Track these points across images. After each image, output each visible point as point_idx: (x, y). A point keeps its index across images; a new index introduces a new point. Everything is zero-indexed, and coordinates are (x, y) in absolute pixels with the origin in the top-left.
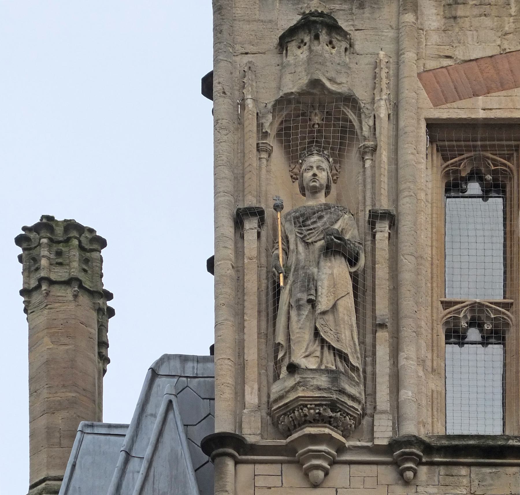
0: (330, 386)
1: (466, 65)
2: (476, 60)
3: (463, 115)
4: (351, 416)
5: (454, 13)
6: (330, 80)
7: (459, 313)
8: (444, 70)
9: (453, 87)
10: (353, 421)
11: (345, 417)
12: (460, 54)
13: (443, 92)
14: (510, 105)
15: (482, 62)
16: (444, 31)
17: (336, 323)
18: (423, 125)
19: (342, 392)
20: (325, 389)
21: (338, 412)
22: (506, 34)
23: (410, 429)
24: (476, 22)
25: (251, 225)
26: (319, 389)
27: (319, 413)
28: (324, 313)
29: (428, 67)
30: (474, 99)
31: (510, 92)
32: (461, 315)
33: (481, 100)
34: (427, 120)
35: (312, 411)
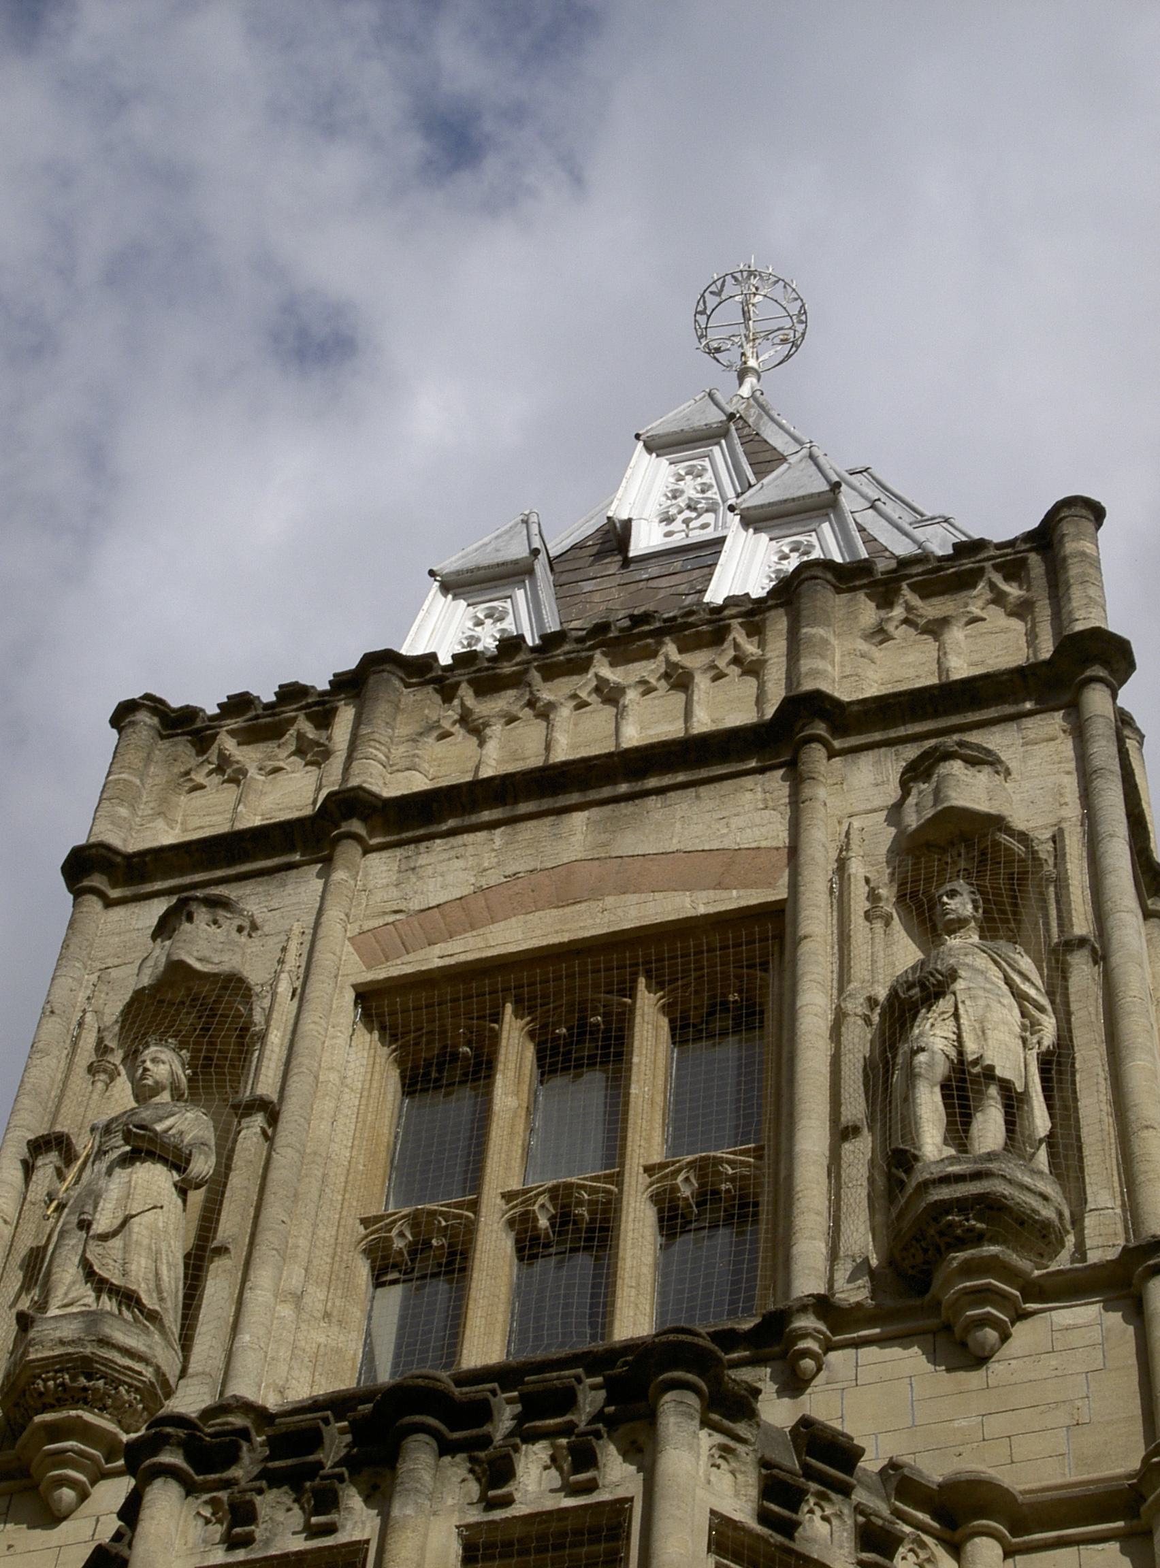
0: (82, 1335)
1: (422, 915)
2: (438, 906)
3: (409, 969)
4: (130, 1386)
5: (412, 865)
6: (200, 960)
7: (390, 1231)
8: (391, 927)
9: (398, 942)
10: (133, 1395)
11: (116, 1388)
12: (415, 905)
13: (383, 950)
14: (482, 945)
15: (446, 907)
16: (397, 885)
17: (126, 1248)
18: (350, 995)
19: (104, 1342)
20: (73, 1341)
21: (98, 1379)
22: (485, 870)
23: (243, 1388)
24: (442, 868)
25: (49, 1162)
26: (62, 1342)
27: (63, 1384)
28: (104, 1237)
29: (365, 928)
30: (428, 949)
31: (481, 931)
32: (394, 1233)
33: (437, 949)
34: (354, 986)
35: (51, 1383)
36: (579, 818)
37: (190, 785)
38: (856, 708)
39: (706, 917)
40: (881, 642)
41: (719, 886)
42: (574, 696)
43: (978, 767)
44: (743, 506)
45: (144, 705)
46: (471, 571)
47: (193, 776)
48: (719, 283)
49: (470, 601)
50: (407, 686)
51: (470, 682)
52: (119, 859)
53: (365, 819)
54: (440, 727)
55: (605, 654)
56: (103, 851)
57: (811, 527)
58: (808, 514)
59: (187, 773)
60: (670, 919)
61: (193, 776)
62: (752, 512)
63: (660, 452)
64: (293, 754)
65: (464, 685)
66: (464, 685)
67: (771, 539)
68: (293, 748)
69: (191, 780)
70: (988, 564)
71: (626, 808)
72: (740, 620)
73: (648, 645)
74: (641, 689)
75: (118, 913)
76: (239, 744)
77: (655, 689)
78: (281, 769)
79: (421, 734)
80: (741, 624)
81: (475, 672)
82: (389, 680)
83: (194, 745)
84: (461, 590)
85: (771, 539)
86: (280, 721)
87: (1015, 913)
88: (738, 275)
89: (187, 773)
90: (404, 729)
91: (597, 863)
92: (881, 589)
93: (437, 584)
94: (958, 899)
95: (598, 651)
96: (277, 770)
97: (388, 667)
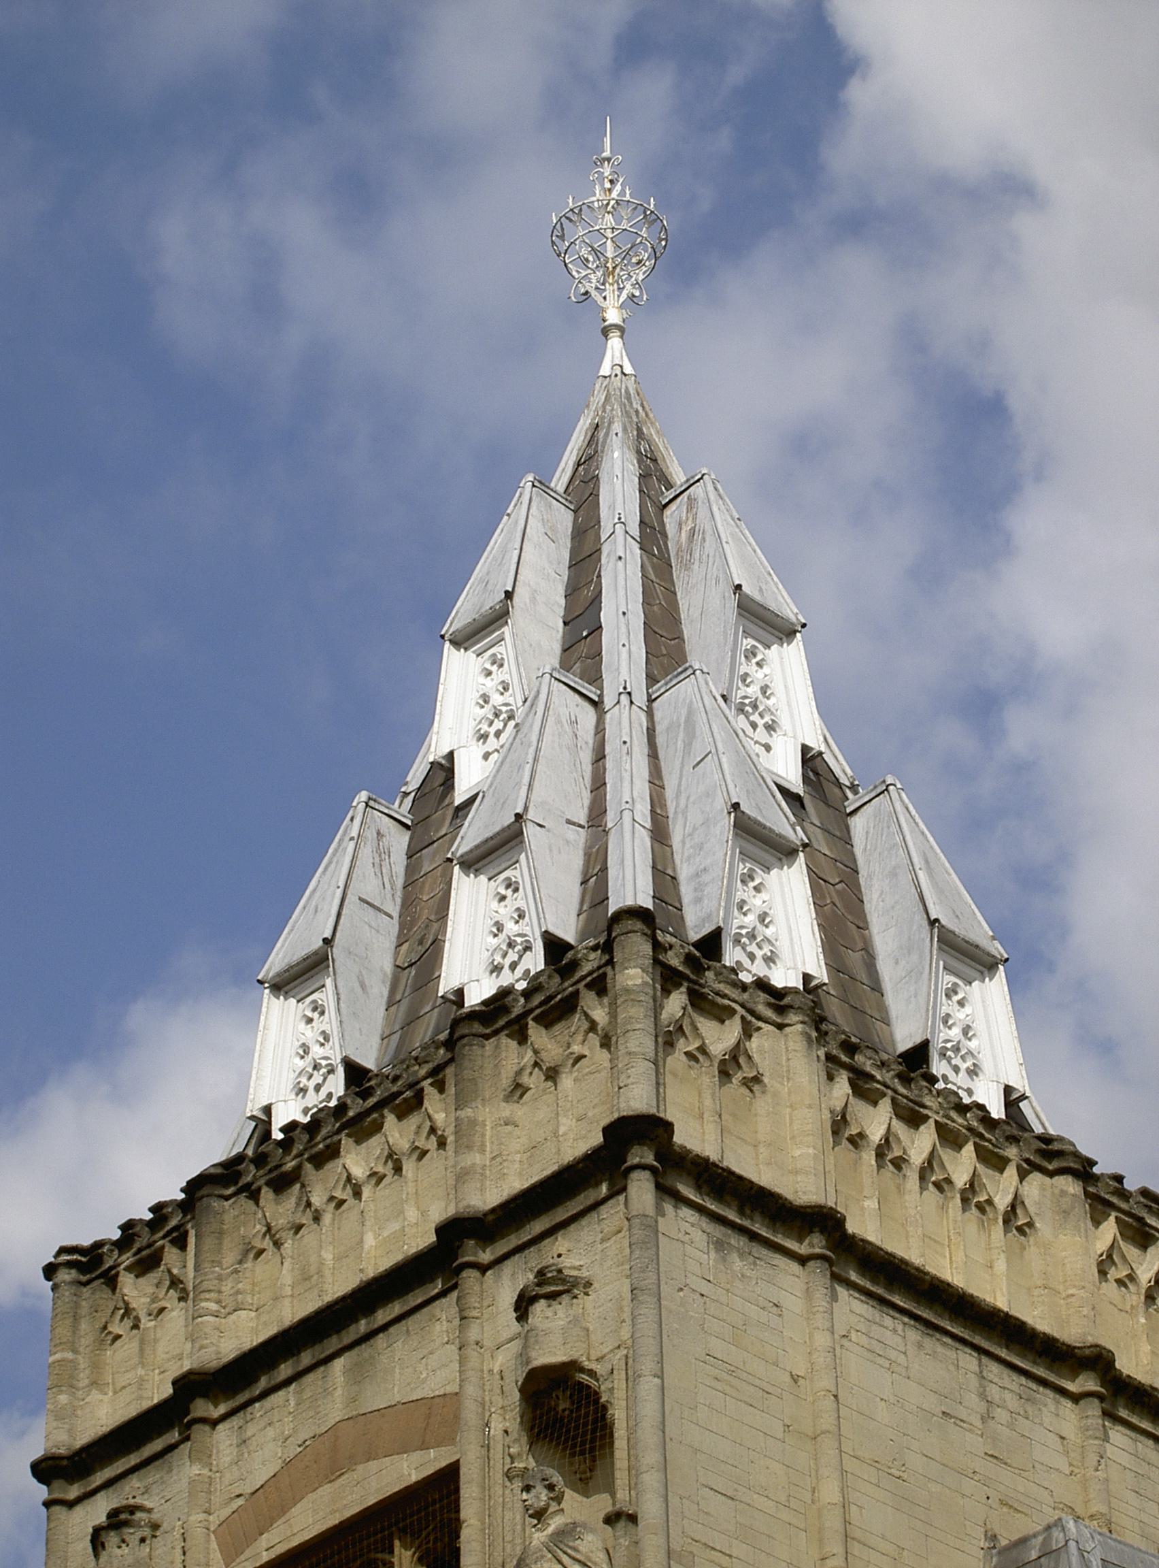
36: (339, 1364)
37: (110, 1337)
38: (491, 1217)
39: (417, 1483)
40: (521, 1096)
41: (424, 1447)
42: (332, 1198)
43: (558, 1299)
44: (458, 854)
45: (60, 1264)
46: (287, 970)
47: (110, 1329)
48: (558, 226)
49: (299, 997)
50: (227, 1198)
51: (268, 1184)
52: (65, 1462)
53: (205, 1395)
54: (253, 1247)
55: (348, 1135)
56: (50, 1462)
57: (514, 860)
58: (508, 846)
59: (105, 1327)
60: (396, 1490)
61: (110, 1329)
62: (465, 858)
63: (466, 645)
64: (170, 1288)
65: (265, 1190)
66: (265, 1190)
67: (490, 879)
68: (168, 1283)
69: (110, 1333)
70: (581, 986)
71: (364, 1350)
72: (429, 1081)
73: (375, 1120)
74: (373, 1181)
75: (79, 1510)
76: (137, 1277)
77: (385, 1176)
78: (164, 1308)
79: (240, 1262)
80: (431, 1084)
81: (270, 1171)
82: (209, 1206)
83: (107, 1285)
84: (288, 987)
85: (490, 879)
86: (156, 1251)
87: (592, 1449)
88: (570, 215)
89: (105, 1327)
90: (230, 1258)
91: (351, 1422)
92: (516, 1027)
93: (267, 991)
94: (533, 1492)
95: (343, 1135)
96: (162, 1310)
97: (204, 1191)
